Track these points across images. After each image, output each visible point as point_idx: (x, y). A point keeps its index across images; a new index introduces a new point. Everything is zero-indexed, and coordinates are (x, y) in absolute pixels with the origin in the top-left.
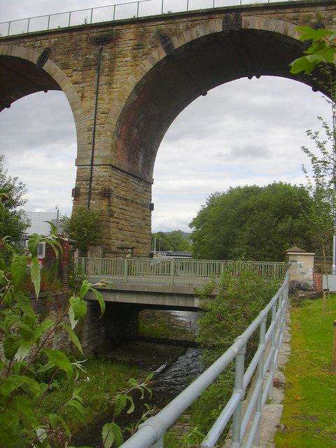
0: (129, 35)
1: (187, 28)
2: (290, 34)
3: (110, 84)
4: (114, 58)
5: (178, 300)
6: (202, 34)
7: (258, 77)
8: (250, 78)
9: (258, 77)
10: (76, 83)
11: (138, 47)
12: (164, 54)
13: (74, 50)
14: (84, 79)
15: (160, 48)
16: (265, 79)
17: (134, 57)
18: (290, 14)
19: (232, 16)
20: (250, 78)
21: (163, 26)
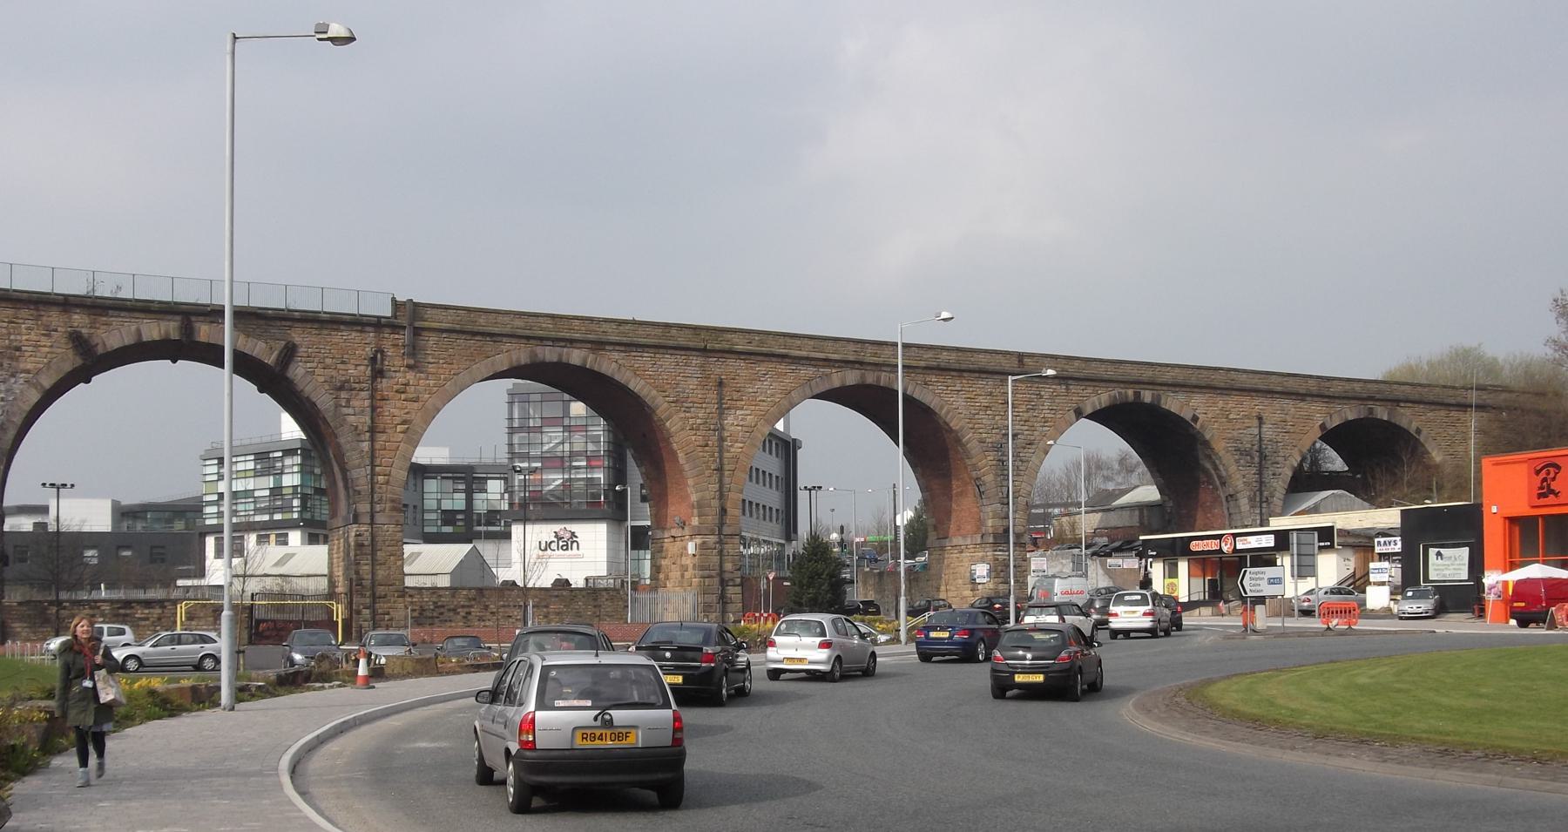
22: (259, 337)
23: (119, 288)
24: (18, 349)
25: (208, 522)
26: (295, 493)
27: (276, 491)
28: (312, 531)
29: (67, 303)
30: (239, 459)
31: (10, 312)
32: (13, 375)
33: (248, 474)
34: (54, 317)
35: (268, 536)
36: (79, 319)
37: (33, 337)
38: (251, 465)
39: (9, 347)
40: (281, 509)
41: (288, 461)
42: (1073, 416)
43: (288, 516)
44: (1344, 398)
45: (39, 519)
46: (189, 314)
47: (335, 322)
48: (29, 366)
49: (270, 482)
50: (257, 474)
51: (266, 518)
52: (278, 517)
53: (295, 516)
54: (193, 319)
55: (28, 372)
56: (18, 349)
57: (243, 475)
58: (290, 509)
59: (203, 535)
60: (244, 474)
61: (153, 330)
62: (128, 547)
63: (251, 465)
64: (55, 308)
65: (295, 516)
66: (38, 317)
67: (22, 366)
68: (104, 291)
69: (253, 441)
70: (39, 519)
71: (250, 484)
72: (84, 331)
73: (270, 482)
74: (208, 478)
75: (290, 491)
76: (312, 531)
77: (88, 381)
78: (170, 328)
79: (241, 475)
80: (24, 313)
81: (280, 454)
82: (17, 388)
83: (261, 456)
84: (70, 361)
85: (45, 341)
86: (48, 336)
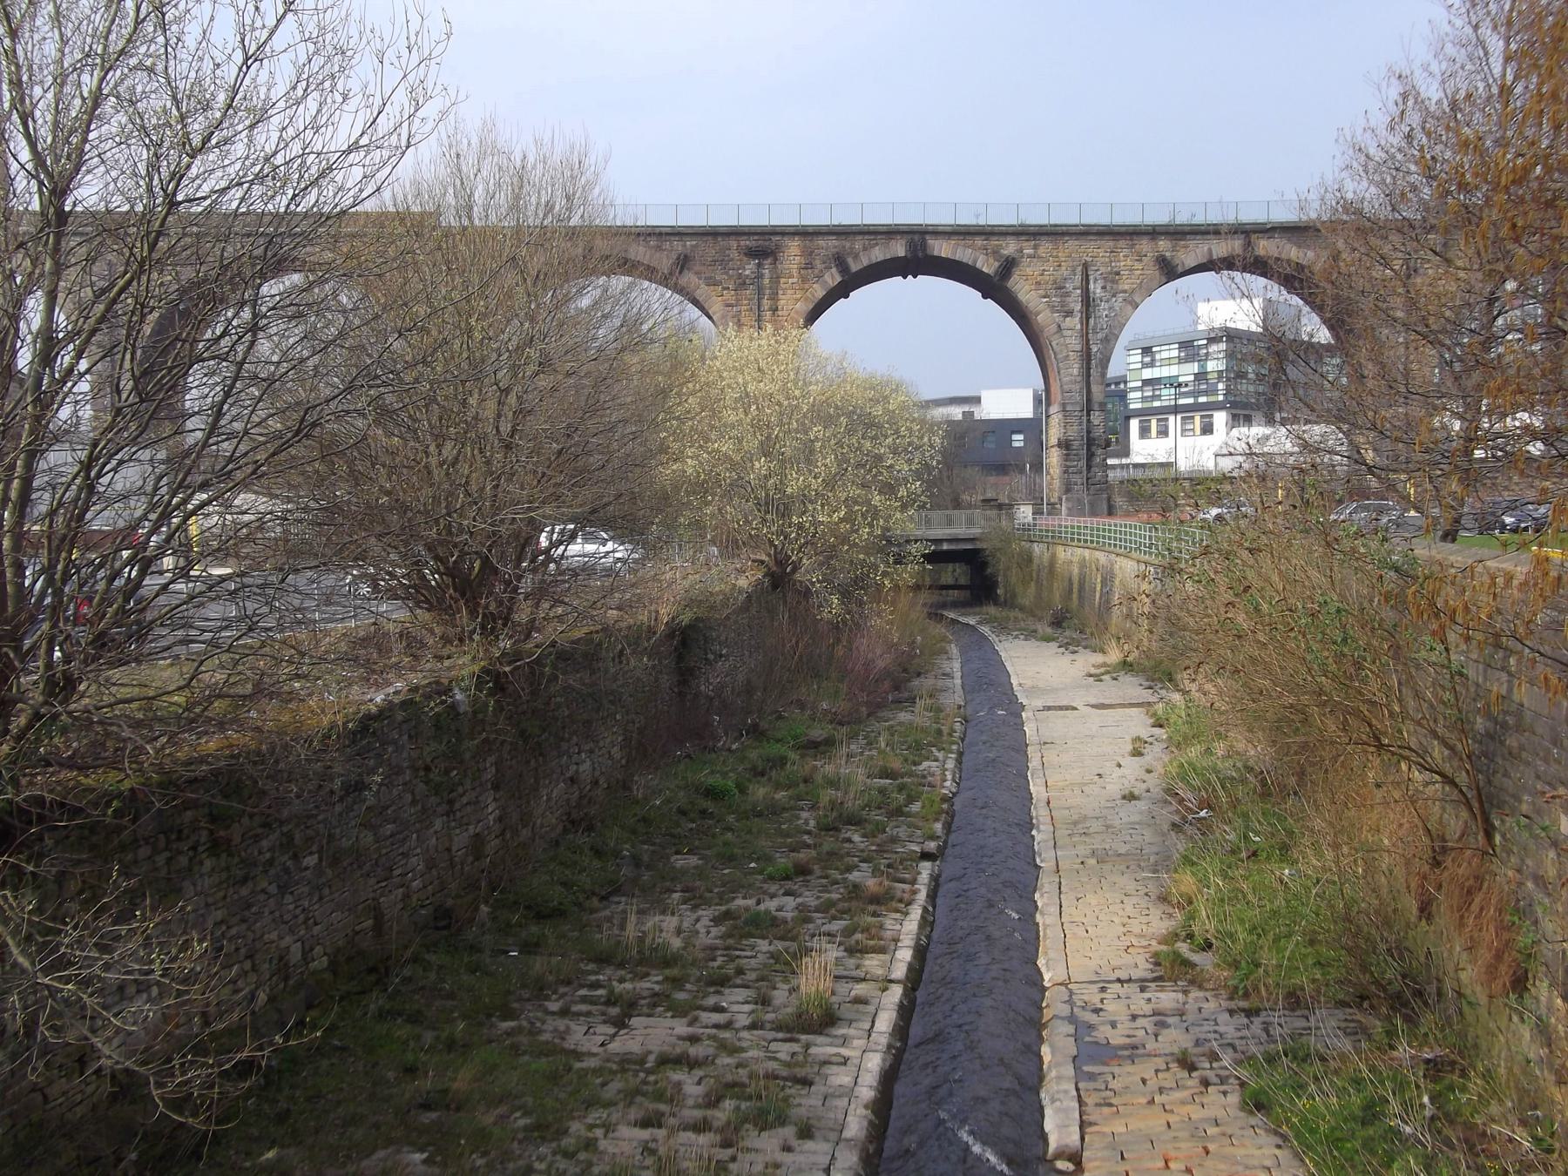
0: (793, 248)
1: (865, 249)
2: (979, 265)
3: (775, 310)
4: (776, 279)
5: (1038, 314)
6: (881, 258)
7: (915, 277)
8: (905, 278)
9: (915, 277)
10: (728, 305)
11: (809, 266)
12: (839, 279)
13: (722, 262)
14: (737, 300)
15: (834, 270)
16: (922, 279)
17: (804, 280)
18: (979, 242)
19: (916, 237)
20: (905, 278)
21: (832, 243)
22: (1308, 247)
23: (977, 216)
24: (1118, 274)
25: (1132, 406)
26: (1220, 378)
27: (1201, 376)
28: (1234, 411)
29: (1154, 232)
30: (1163, 348)
31: (1111, 243)
32: (1114, 296)
33: (1172, 361)
34: (1144, 245)
35: (1193, 417)
36: (1163, 245)
37: (1129, 263)
38: (1175, 353)
39: (1110, 273)
40: (1206, 393)
41: (1214, 348)
42: (1153, 272)
43: (1212, 399)
44: (1063, 234)
45: (966, 409)
46: (918, 235)
47: (1055, 233)
48: (1126, 287)
49: (1194, 367)
50: (1181, 361)
51: (1191, 401)
52: (1202, 399)
53: (1221, 398)
54: (928, 237)
55: (1125, 292)
56: (1118, 274)
57: (1167, 362)
58: (1215, 392)
59: (1128, 418)
60: (1169, 362)
61: (1220, 249)
62: (1019, 432)
63: (1175, 353)
64: (1146, 237)
65: (1221, 398)
66: (1133, 246)
67: (1121, 287)
68: (1182, 218)
69: (1177, 331)
70: (966, 409)
71: (1173, 370)
72: (1168, 254)
73: (1194, 367)
74: (1132, 367)
75: (1216, 375)
76: (1234, 411)
77: (985, 297)
78: (1235, 246)
79: (1164, 362)
80: (1122, 243)
81: (1205, 342)
82: (1117, 306)
83: (1186, 345)
84: (833, 278)
85: (1138, 266)
86: (1140, 260)
